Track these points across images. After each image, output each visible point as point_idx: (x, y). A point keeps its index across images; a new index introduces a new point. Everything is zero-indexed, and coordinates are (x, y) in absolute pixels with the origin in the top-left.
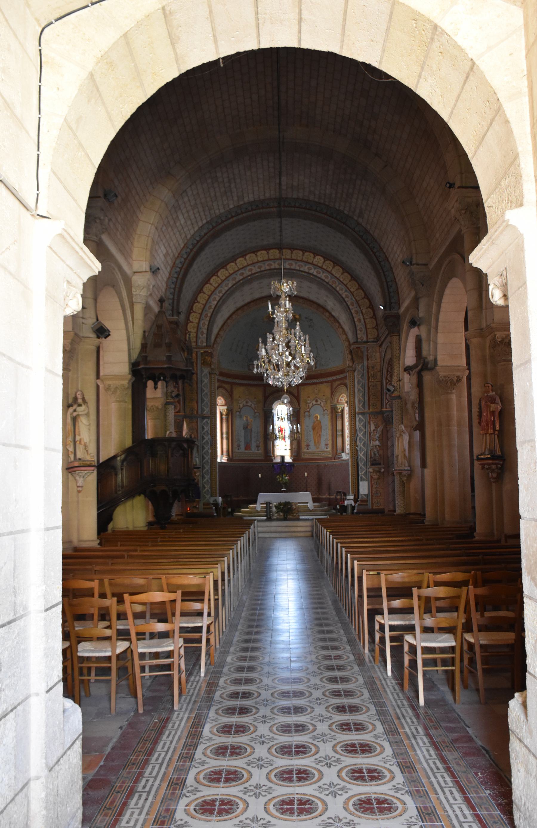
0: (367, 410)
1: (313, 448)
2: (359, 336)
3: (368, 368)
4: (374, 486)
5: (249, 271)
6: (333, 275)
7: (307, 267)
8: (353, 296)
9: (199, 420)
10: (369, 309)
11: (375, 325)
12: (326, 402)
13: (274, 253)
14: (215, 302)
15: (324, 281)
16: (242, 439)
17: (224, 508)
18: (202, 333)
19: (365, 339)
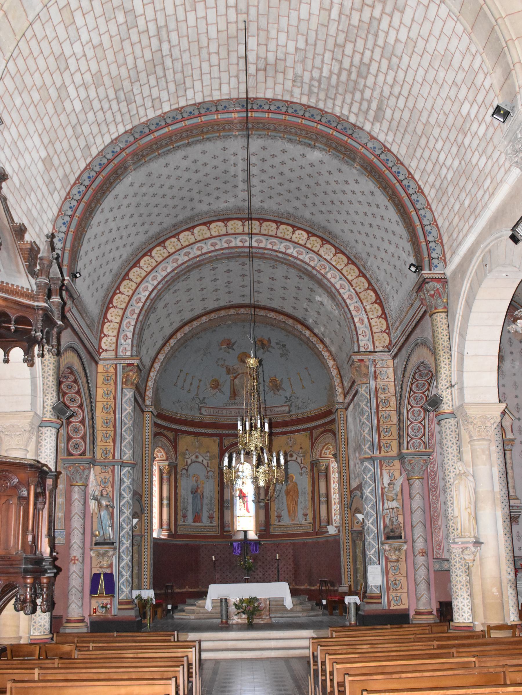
0: (377, 453)
1: (286, 520)
2: (361, 344)
3: (377, 391)
4: (391, 573)
5: (198, 249)
6: (321, 256)
7: (283, 245)
8: (352, 286)
9: (117, 468)
10: (376, 306)
11: (385, 327)
12: (303, 456)
13: (236, 226)
14: (147, 293)
15: (308, 264)
16: (190, 508)
17: (158, 605)
18: (126, 337)
19: (371, 348)
